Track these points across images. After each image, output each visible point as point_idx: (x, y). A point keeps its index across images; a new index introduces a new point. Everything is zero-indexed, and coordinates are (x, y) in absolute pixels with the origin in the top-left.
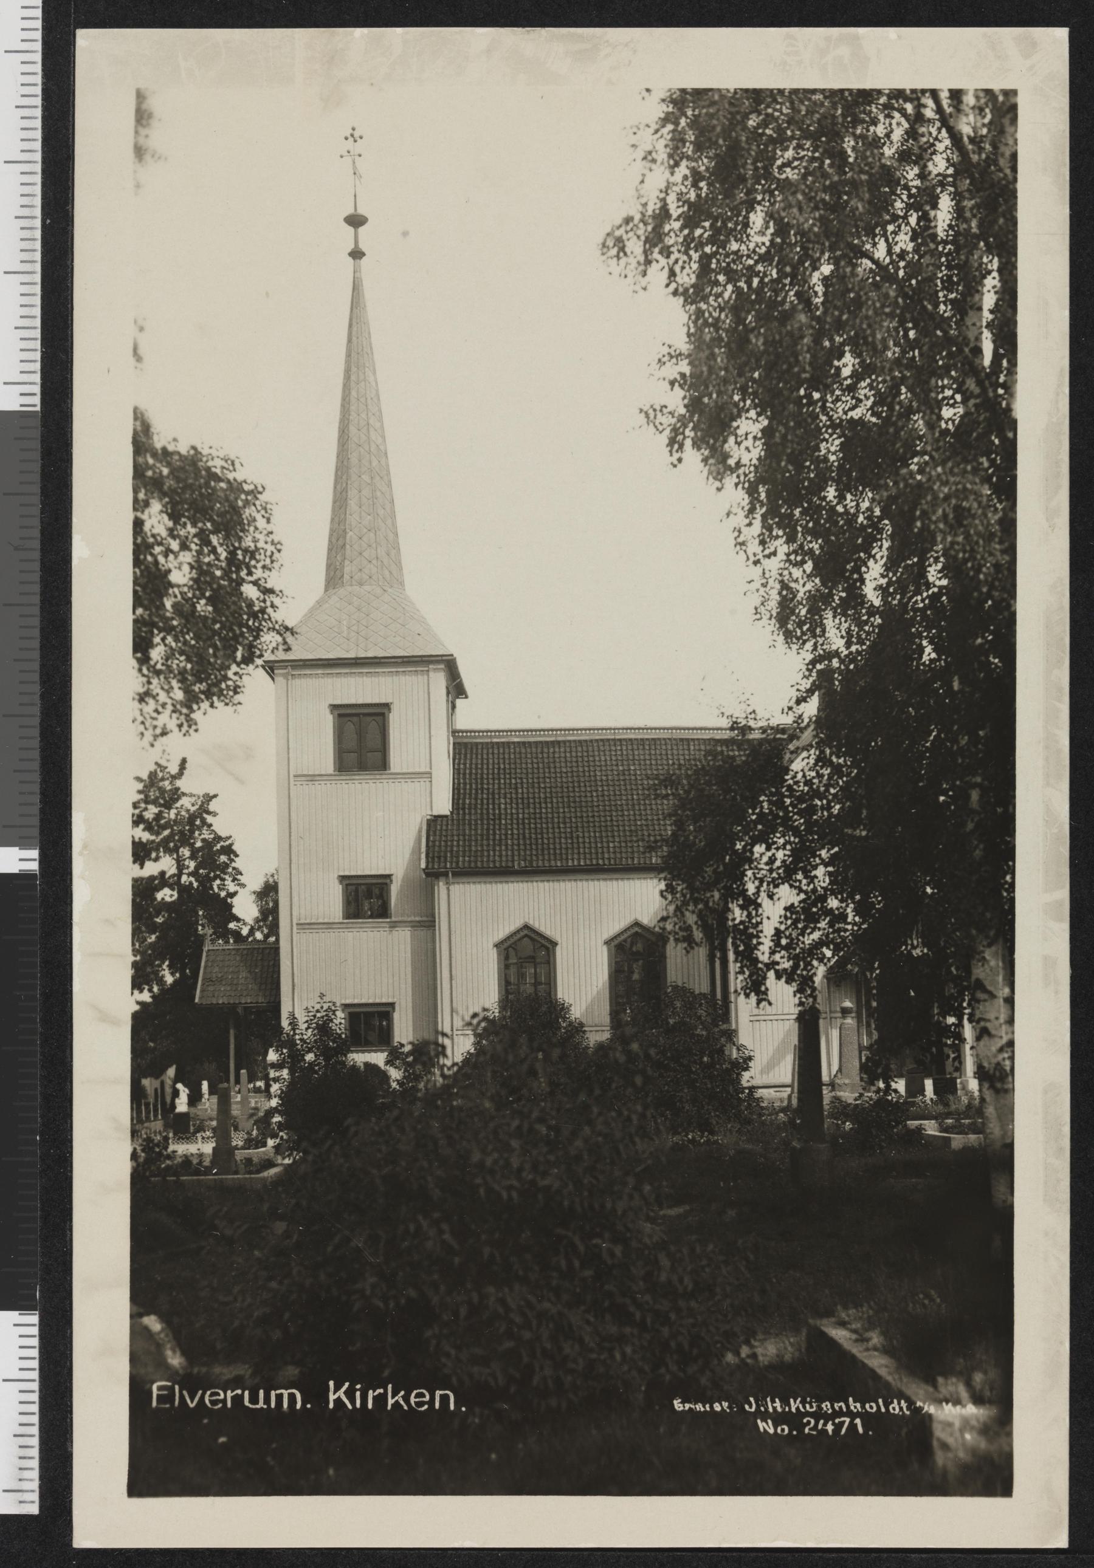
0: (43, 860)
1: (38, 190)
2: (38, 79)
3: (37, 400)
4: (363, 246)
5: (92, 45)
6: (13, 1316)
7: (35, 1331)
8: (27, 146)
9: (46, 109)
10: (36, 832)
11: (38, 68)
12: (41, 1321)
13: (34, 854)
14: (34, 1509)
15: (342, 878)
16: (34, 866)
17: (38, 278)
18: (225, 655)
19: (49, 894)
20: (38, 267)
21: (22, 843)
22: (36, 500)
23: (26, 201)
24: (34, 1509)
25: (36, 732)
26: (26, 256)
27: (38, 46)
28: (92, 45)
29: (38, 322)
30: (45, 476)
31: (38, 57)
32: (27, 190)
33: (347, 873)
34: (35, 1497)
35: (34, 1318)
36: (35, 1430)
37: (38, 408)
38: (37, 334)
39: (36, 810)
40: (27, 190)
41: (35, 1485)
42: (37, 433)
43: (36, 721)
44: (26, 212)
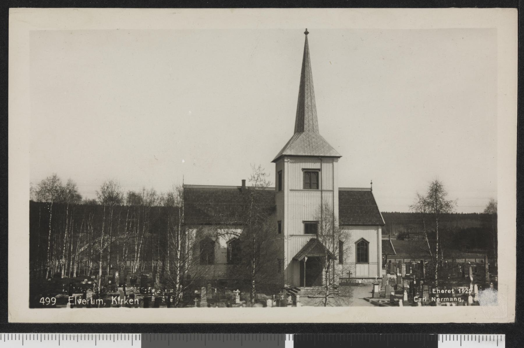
0: (289, 333)
1: (68, 334)
2: (32, 334)
3: (138, 335)
4: (305, 35)
5: (12, 318)
6: (440, 343)
7: (444, 335)
8: (90, 338)
9: (42, 332)
10: (280, 335)
11: (28, 334)
12: (441, 333)
13: (287, 335)
14: (504, 336)
15: (304, 222)
16: (291, 335)
17: (98, 334)
18: (71, 305)
19: (299, 330)
20: (94, 334)
21: (284, 339)
22: (171, 334)
23: (72, 338)
24: (504, 336)
25: (247, 335)
26: (90, 338)
27: (21, 334)
28: (12, 318)
29: (112, 334)
30: (169, 332)
31: (25, 334)
32: (68, 338)
33: (305, 220)
34: (499, 335)
35: (440, 336)
36: (477, 335)
37: (141, 334)
38: (116, 334)
39: (273, 335)
40: (68, 338)
41: (496, 335)
42: (149, 335)
43: (244, 335)
44: (76, 338)
